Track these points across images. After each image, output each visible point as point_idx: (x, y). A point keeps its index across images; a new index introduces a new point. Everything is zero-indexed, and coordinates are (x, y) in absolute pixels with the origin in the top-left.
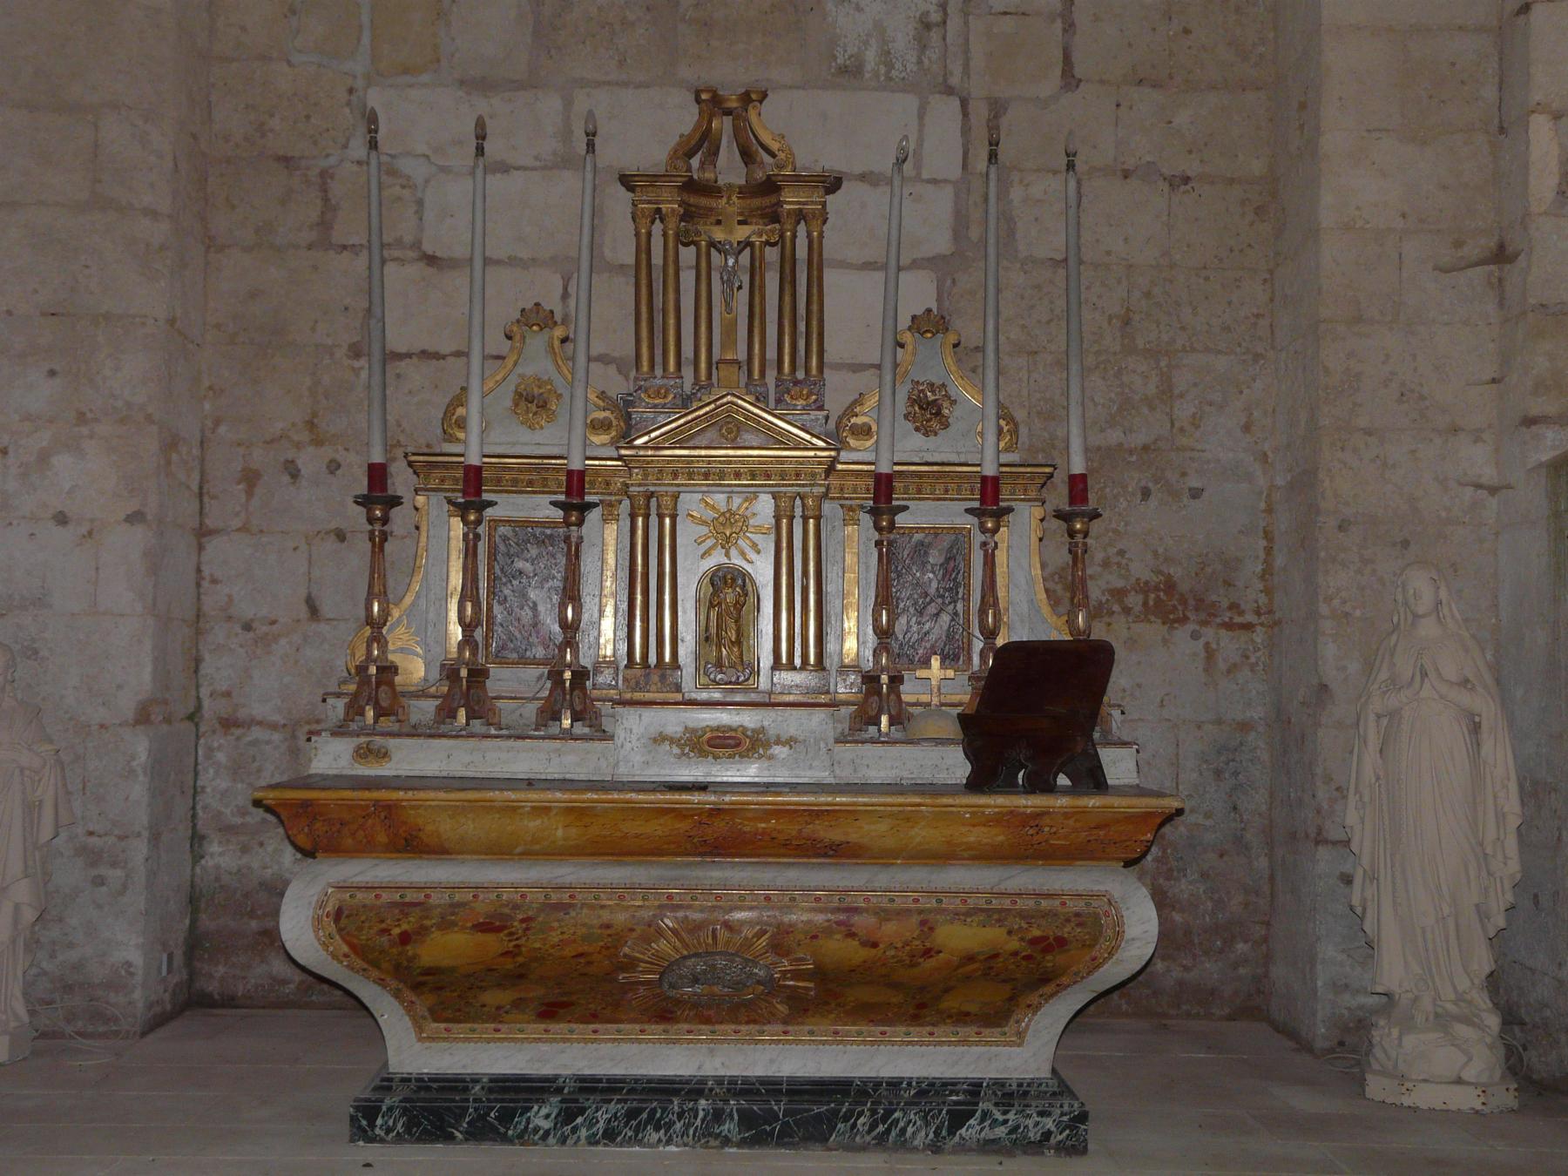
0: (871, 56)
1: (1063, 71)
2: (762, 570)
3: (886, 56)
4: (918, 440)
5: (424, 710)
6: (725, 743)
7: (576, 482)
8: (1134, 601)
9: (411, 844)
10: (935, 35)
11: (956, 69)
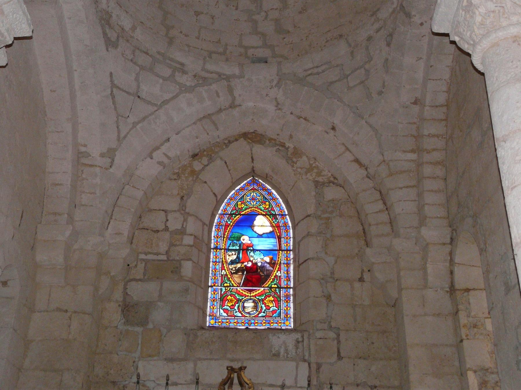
0: (282, 351)
3: (286, 351)
10: (300, 345)
11: (307, 354)
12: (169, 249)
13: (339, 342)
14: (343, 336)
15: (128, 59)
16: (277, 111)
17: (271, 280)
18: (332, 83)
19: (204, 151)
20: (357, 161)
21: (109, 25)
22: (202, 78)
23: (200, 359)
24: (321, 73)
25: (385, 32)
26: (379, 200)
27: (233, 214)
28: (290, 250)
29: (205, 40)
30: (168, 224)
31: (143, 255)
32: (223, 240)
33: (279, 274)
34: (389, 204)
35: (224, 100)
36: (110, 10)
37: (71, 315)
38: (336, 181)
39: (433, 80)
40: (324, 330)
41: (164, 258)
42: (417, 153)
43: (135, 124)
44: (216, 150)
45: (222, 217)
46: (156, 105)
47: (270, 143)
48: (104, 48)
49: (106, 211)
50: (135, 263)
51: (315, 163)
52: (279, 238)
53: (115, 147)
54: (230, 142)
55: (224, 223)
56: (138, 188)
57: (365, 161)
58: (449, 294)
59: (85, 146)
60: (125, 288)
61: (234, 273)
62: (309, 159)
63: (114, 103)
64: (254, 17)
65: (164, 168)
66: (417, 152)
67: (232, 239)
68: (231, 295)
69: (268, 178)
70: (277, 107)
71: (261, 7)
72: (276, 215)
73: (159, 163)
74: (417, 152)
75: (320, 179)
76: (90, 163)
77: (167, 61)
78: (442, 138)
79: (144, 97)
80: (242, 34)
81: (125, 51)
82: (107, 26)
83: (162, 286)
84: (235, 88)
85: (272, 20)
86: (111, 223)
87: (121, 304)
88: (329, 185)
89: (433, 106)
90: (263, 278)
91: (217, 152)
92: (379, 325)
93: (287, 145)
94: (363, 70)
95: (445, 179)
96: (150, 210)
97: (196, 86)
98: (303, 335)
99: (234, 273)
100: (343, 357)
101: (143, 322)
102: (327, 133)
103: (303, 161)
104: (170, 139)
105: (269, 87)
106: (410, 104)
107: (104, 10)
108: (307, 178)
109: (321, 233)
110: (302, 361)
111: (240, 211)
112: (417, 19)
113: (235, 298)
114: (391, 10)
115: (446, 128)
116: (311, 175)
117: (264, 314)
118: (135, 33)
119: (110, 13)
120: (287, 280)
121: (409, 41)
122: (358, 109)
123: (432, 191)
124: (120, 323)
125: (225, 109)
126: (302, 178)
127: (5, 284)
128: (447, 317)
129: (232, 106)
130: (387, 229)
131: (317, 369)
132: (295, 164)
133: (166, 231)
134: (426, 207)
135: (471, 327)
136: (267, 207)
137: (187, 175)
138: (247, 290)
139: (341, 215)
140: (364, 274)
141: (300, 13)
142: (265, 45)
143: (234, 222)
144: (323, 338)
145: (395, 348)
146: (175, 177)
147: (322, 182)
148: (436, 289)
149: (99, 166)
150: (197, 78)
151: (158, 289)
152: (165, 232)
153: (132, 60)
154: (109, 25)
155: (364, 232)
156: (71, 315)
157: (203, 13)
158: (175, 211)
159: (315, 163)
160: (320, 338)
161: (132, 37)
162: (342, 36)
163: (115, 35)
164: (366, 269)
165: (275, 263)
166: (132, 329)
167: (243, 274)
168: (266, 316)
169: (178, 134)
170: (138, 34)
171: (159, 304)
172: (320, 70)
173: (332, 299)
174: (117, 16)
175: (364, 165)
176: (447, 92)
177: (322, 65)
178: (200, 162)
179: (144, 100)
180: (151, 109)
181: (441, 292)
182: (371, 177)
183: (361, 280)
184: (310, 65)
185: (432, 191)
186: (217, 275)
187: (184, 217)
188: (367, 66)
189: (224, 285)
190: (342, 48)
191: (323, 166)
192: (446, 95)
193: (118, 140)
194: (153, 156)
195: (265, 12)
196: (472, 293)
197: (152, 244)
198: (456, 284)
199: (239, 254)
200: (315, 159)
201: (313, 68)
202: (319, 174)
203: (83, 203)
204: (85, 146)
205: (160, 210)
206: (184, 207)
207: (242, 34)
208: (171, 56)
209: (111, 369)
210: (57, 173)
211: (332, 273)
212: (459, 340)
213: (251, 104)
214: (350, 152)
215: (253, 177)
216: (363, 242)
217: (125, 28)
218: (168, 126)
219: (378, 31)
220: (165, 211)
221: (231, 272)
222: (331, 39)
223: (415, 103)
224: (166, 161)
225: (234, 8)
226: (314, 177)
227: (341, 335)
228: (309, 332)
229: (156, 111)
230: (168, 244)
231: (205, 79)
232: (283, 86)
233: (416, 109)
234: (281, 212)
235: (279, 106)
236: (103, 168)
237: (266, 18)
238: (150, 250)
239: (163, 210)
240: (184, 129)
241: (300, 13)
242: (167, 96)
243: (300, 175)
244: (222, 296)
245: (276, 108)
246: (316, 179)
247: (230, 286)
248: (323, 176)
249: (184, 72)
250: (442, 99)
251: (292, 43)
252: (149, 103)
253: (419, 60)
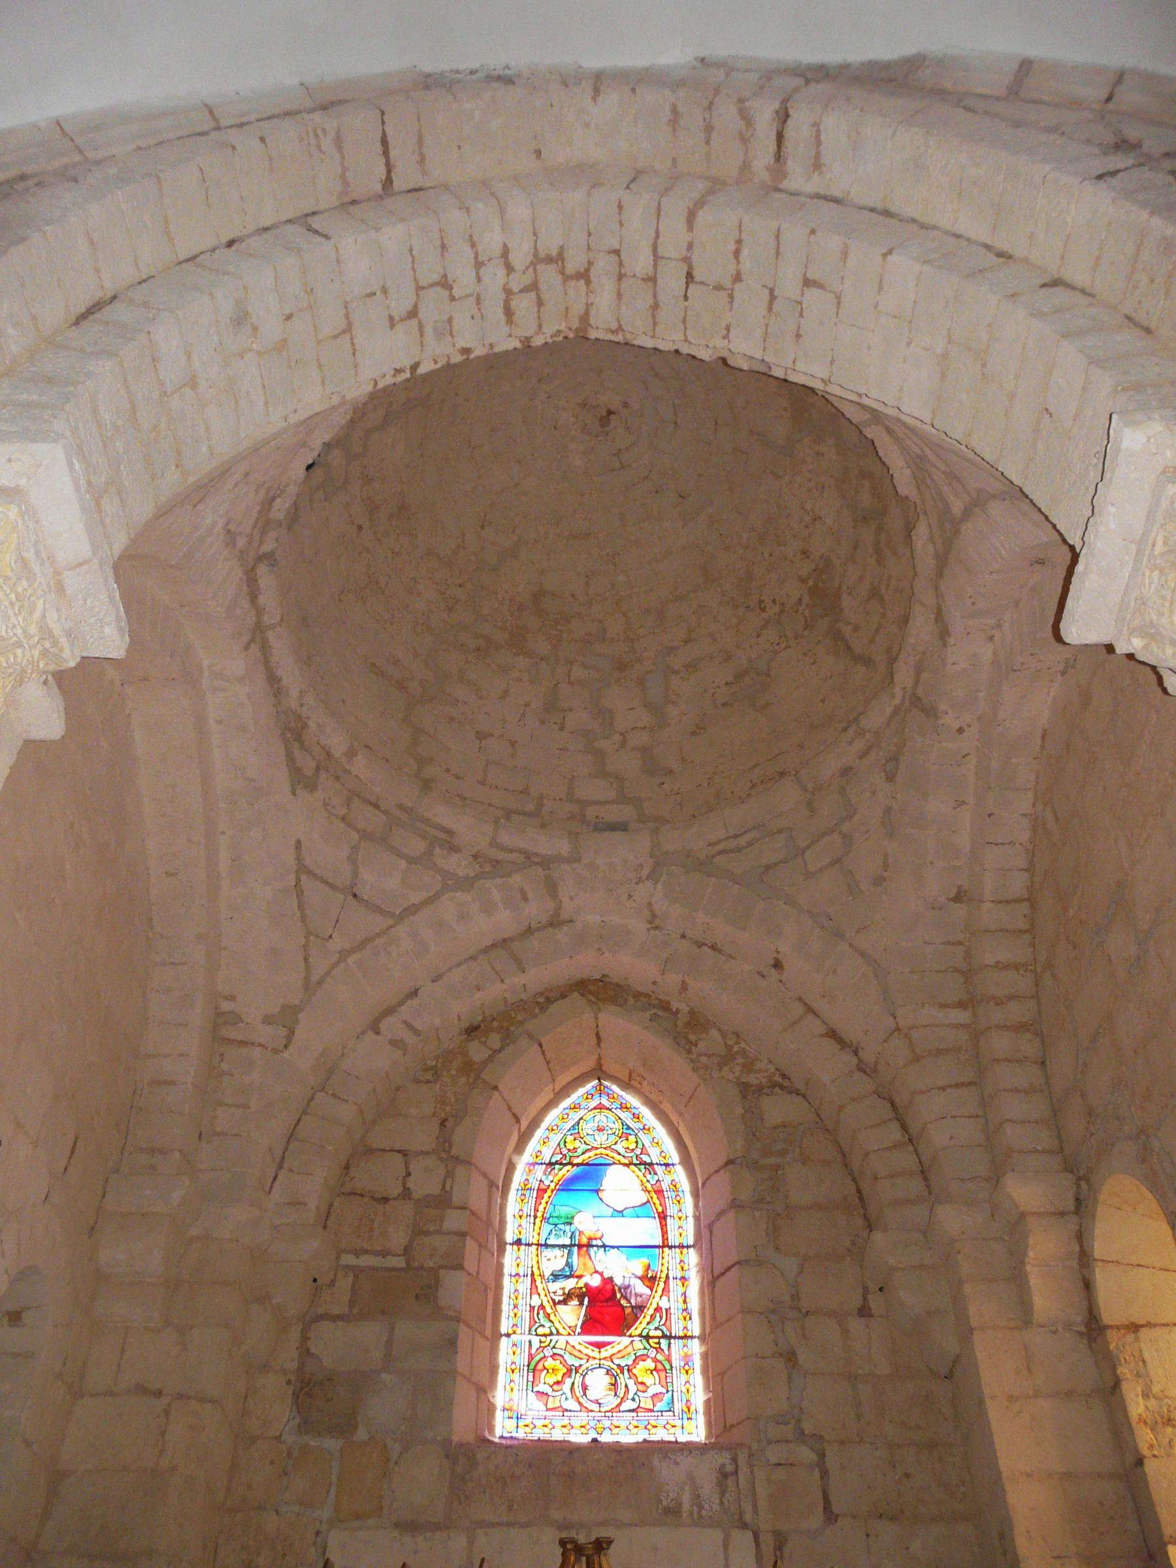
1: (825, 1509)
3: (697, 1499)
10: (730, 1481)
12: (411, 1242)
13: (825, 1474)
14: (831, 1453)
15: (337, 816)
16: (652, 932)
17: (648, 1319)
18: (768, 868)
19: (493, 1019)
20: (833, 1034)
21: (302, 744)
22: (491, 861)
23: (481, 1524)
24: (745, 848)
25: (881, 754)
26: (890, 1120)
27: (556, 1163)
28: (688, 1247)
29: (497, 787)
30: (411, 1183)
31: (352, 1255)
32: (534, 1223)
33: (664, 1304)
34: (914, 1128)
35: (536, 909)
36: (304, 711)
37: (169, 1405)
38: (786, 1083)
39: (996, 844)
40: (787, 1441)
41: (399, 1262)
42: (970, 1009)
43: (344, 954)
44: (520, 1018)
45: (530, 1171)
46: (391, 914)
47: (636, 1002)
48: (287, 788)
49: (270, 1149)
50: (332, 1275)
51: (737, 1043)
52: (663, 1217)
53: (297, 1002)
54: (549, 1001)
55: (535, 1185)
56: (346, 1098)
57: (851, 1033)
58: (1085, 1341)
59: (232, 998)
60: (305, 1339)
61: (560, 1302)
62: (724, 1035)
63: (301, 906)
64: (596, 744)
65: (404, 1055)
66: (970, 1005)
67: (555, 1221)
68: (554, 1356)
69: (633, 1083)
70: (651, 923)
71: (611, 724)
72: (651, 1164)
73: (395, 1043)
74: (970, 1005)
75: (752, 1079)
76: (240, 1037)
77: (418, 824)
78: (1026, 971)
79: (366, 898)
80: (573, 776)
81: (330, 799)
82: (296, 743)
83: (392, 1330)
84: (561, 883)
85: (634, 749)
86: (280, 1178)
87: (293, 1377)
88: (772, 1092)
89: (1000, 902)
90: (629, 1314)
91: (522, 1023)
92: (918, 1427)
93: (675, 1005)
94: (836, 835)
95: (1043, 1063)
96: (370, 1151)
97: (477, 877)
98: (736, 1455)
99: (560, 1302)
100: (837, 1516)
101: (344, 1426)
102: (763, 976)
103: (711, 1041)
104: (419, 991)
105: (634, 881)
106: (946, 901)
107: (292, 711)
108: (723, 1077)
109: (762, 1200)
110: (737, 1527)
111: (570, 1157)
112: (950, 720)
113: (564, 1363)
114: (889, 710)
115: (1032, 949)
116: (731, 1069)
117: (634, 1405)
118: (352, 764)
119: (304, 719)
120: (685, 1318)
121: (937, 767)
122: (831, 920)
123: (1017, 1090)
124: (287, 1428)
125: (538, 929)
126: (712, 1078)
127: (15, 1318)
128: (1090, 1400)
129: (555, 922)
130: (916, 1186)
131: (775, 1550)
132: (693, 1047)
133: (404, 1199)
134: (1009, 1129)
135: (1156, 1422)
136: (633, 1146)
137: (454, 1072)
138: (591, 1344)
139: (805, 1160)
140: (870, 1297)
141: (693, 733)
142: (623, 798)
143: (559, 1181)
144: (786, 1465)
145: (963, 1489)
146: (429, 1076)
147: (755, 1085)
148: (1054, 1328)
149: (260, 1045)
150: (480, 860)
151: (385, 1338)
152: (403, 1201)
153: (343, 819)
154: (302, 744)
155: (861, 1198)
156: (169, 1405)
157: (492, 736)
158: (427, 1153)
159: (739, 1043)
160: (779, 1465)
161: (345, 771)
162: (786, 774)
163: (313, 764)
164: (873, 1287)
165: (656, 1277)
166: (317, 1444)
167: (581, 1304)
168: (639, 1410)
169: (436, 981)
170: (361, 765)
171: (386, 1377)
172: (742, 841)
173: (800, 1362)
174: (319, 725)
175: (850, 1044)
176: (1026, 870)
177: (745, 832)
178: (484, 1043)
179: (366, 903)
180: (380, 922)
181: (1067, 1335)
182: (868, 1071)
183: (864, 1312)
184: (721, 834)
185: (1017, 1090)
186: (520, 1307)
187: (447, 1166)
188: (845, 827)
189: (536, 1330)
190: (788, 795)
191: (755, 1051)
192: (1025, 876)
193: (306, 987)
194: (380, 1028)
195: (621, 734)
196: (1144, 1333)
197: (371, 1230)
198: (1102, 1313)
199: (570, 1254)
200: (738, 1036)
201: (727, 838)
202: (748, 1067)
203: (218, 1129)
204: (232, 998)
205: (392, 1150)
206: (447, 1144)
207: (573, 776)
208: (426, 814)
209: (259, 1554)
210: (166, 1056)
211: (796, 1297)
212: (1130, 1460)
213: (594, 918)
214: (817, 1016)
215: (600, 1081)
216: (860, 1222)
217: (333, 752)
218: (416, 961)
219: (863, 755)
220: (404, 1153)
221: (553, 1301)
222: (762, 782)
223: (958, 898)
224: (409, 1038)
225: (557, 727)
226: (737, 1074)
227: (828, 1454)
228: (750, 1448)
229: (392, 927)
230: (409, 1231)
231: (496, 863)
232: (664, 876)
233: (959, 911)
234: (665, 1158)
235: (657, 922)
236: (270, 1049)
237: (624, 743)
238: (366, 1245)
239: (399, 1151)
240: (450, 970)
241: (693, 733)
242: (415, 897)
243: (707, 1070)
244: (532, 1359)
245: (649, 926)
246: (743, 1080)
247: (551, 1334)
248: (759, 1071)
249: (453, 849)
250: (1018, 884)
251: (678, 794)
252: (378, 910)
253: (959, 806)
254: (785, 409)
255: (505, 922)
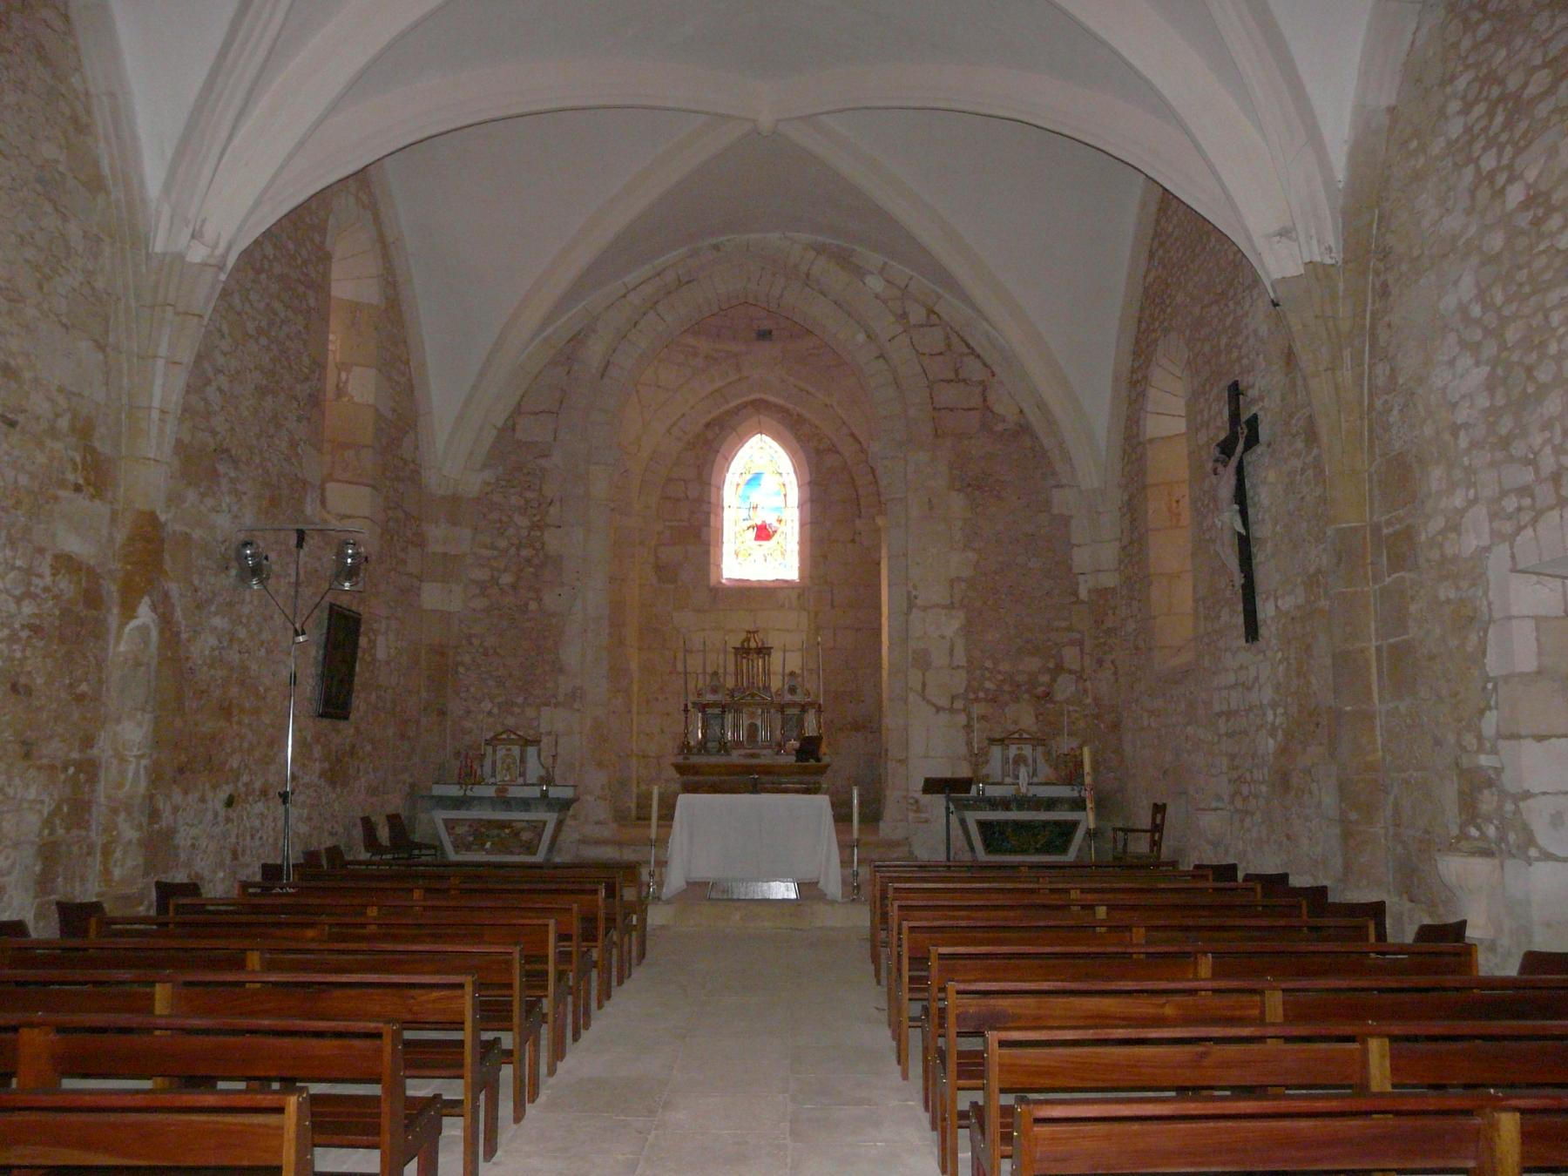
2: (759, 722)
4: (790, 697)
5: (695, 750)
6: (752, 756)
7: (723, 707)
8: (849, 726)
9: (697, 773)
13: (832, 594)
30: (689, 493)
54: (739, 410)
183: (853, 541)
254: (825, 754)
255: (718, 384)
